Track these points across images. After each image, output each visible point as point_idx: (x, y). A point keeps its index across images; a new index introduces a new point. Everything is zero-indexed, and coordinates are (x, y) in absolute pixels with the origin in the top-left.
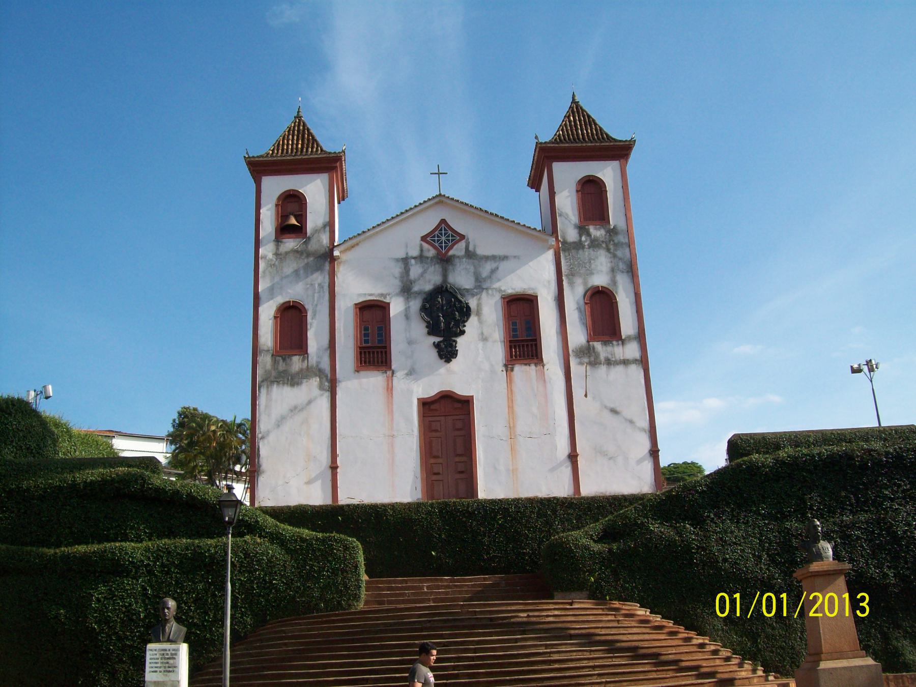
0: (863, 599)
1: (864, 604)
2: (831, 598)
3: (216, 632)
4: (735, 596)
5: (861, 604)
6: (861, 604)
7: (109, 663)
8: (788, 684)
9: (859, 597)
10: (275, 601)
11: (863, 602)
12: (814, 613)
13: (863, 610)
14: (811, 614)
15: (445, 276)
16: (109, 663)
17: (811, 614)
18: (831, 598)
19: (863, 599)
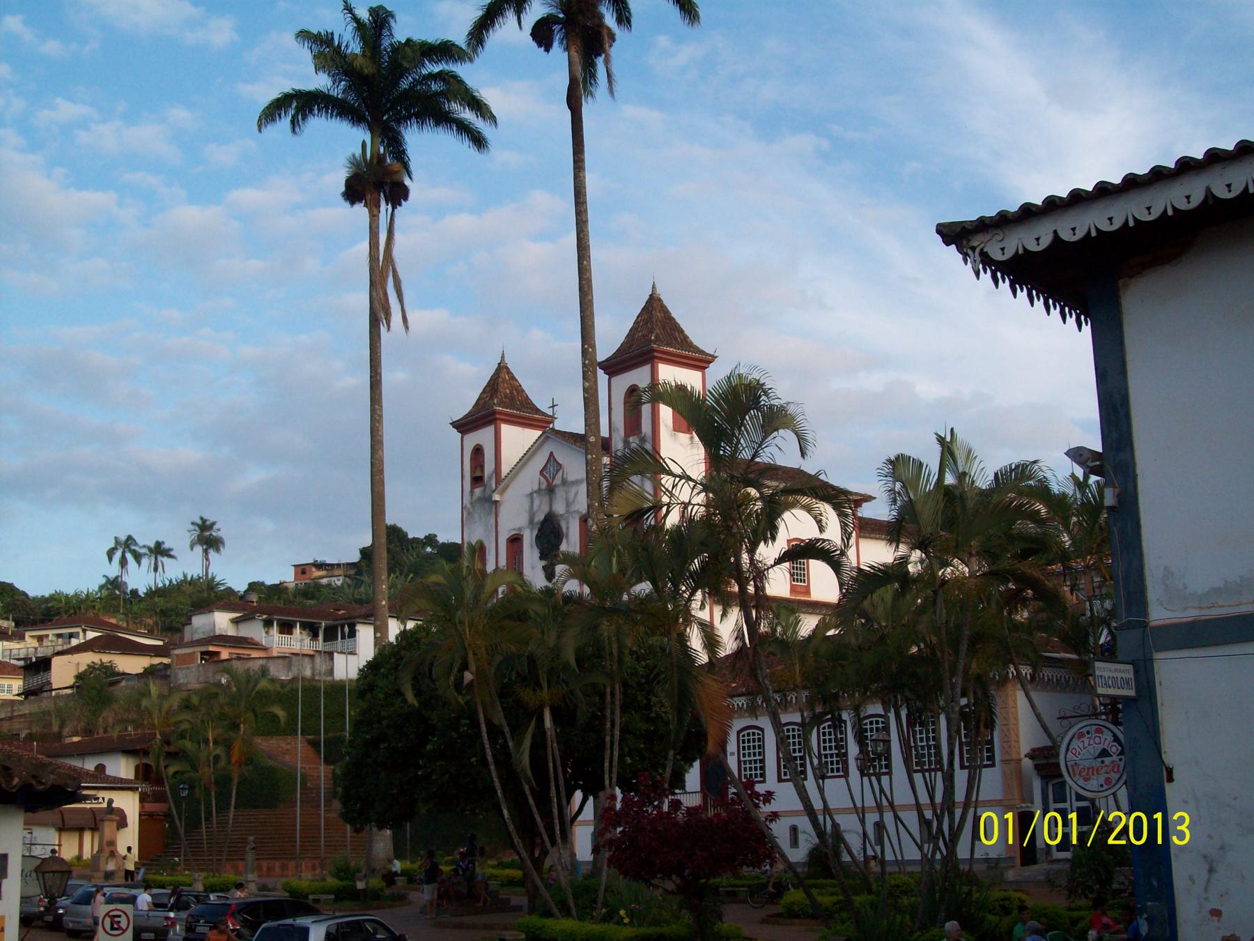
0: (1181, 820)
1: (1183, 828)
2: (1138, 820)
3: (388, 100)
4: (1070, 816)
5: (1179, 828)
6: (1179, 828)
7: (1085, 525)
8: (305, 932)
9: (1175, 817)
10: (1091, 889)
11: (1181, 824)
12: (1114, 839)
13: (1181, 836)
14: (1111, 841)
15: (551, 505)
16: (1085, 525)
17: (1111, 841)
18: (1138, 820)
19: (1181, 820)
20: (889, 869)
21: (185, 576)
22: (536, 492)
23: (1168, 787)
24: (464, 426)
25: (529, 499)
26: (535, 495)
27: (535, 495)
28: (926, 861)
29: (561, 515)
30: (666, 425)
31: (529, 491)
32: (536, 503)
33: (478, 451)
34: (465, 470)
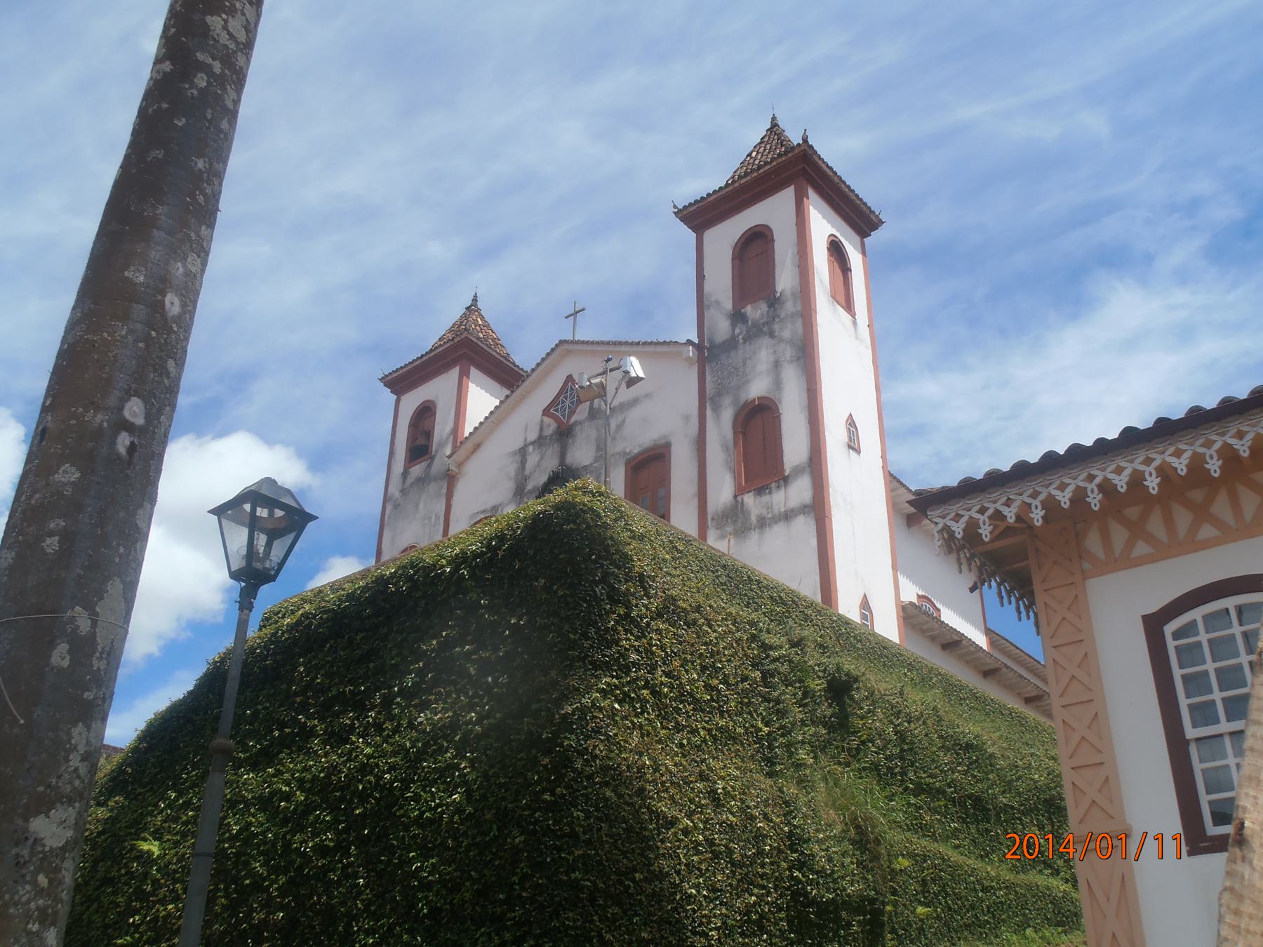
20: (586, 828)
21: (43, 839)
22: (533, 443)
23: (389, 390)
24: (400, 382)
25: (518, 458)
26: (531, 448)
27: (531, 448)
28: (463, 761)
29: (585, 467)
30: (821, 282)
31: (519, 444)
32: (533, 459)
33: (426, 412)
34: (397, 441)
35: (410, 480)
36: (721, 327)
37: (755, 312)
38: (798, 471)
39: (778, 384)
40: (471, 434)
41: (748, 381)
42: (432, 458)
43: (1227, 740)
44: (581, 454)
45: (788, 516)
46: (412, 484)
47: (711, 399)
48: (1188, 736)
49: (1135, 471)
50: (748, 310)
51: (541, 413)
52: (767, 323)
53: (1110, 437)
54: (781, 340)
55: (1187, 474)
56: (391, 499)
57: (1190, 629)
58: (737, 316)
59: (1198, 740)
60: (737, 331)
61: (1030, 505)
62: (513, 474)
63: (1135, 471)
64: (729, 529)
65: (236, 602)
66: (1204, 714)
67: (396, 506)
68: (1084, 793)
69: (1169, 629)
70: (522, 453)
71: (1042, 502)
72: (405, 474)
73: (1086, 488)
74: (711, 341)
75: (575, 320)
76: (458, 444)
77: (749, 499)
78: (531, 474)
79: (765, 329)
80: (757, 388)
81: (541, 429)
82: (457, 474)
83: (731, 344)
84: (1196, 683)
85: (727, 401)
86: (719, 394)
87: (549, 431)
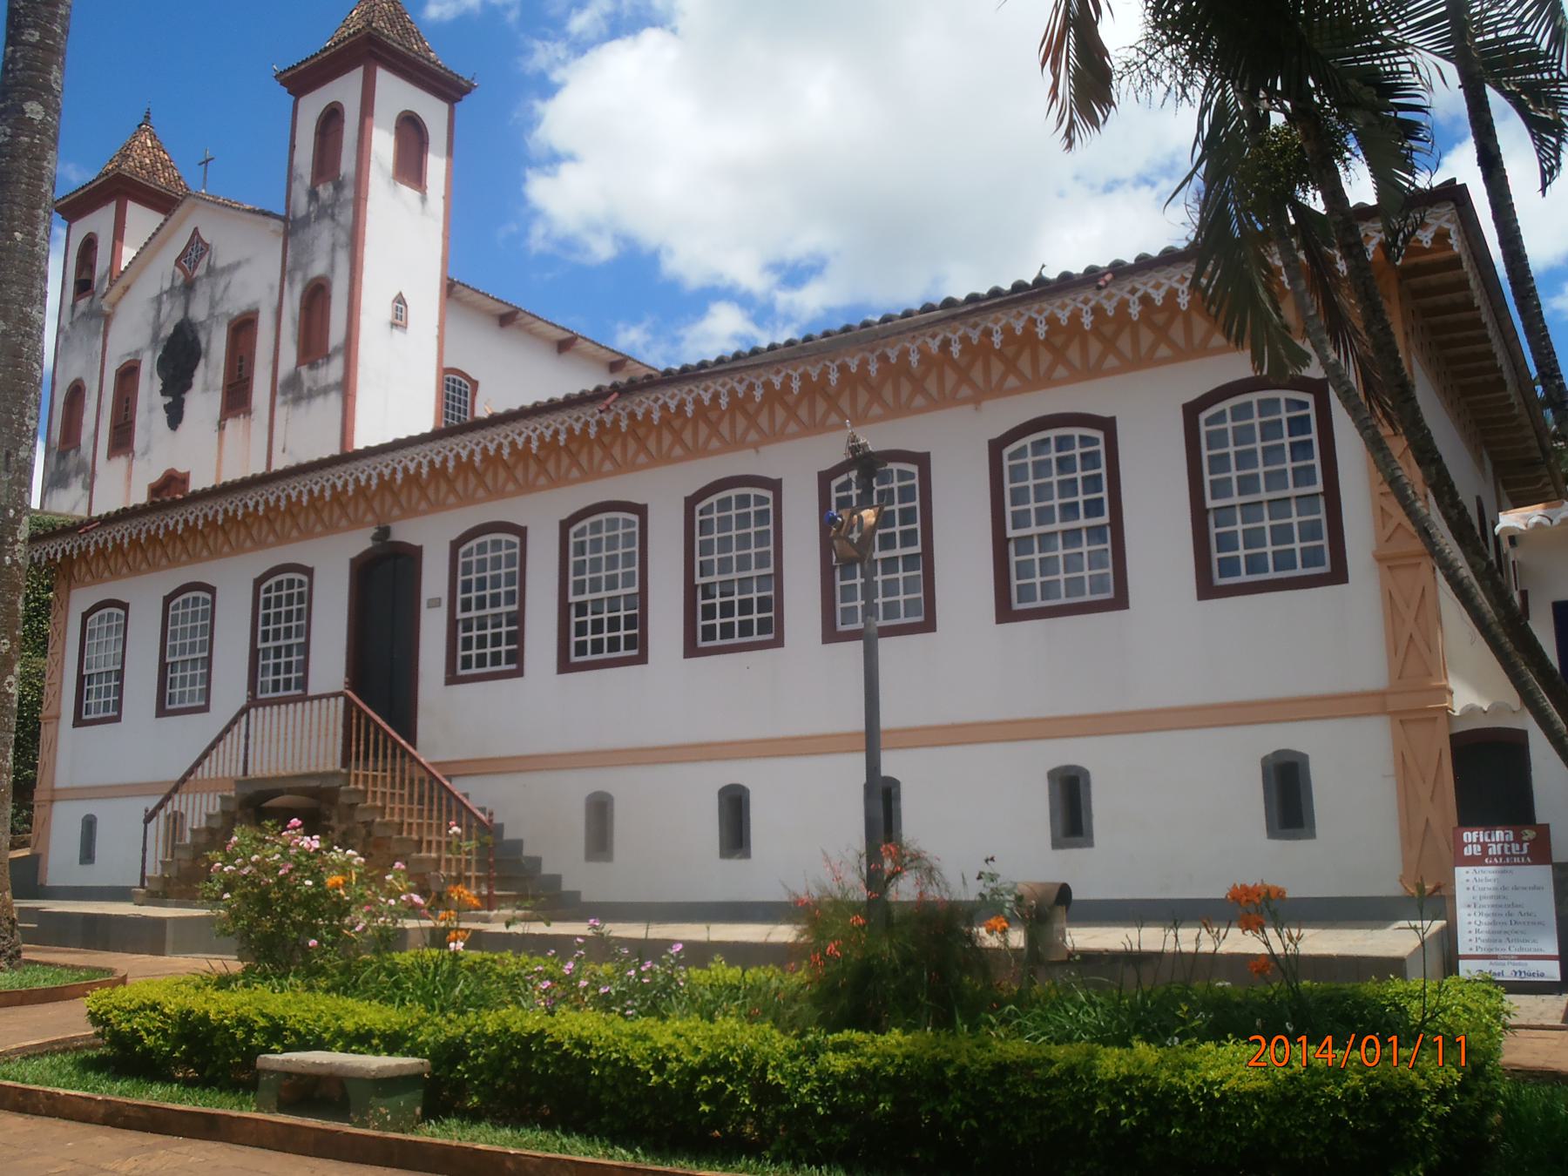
22: (166, 292)
26: (165, 296)
32: (166, 308)
35: (77, 314)
36: (301, 204)
37: (325, 191)
38: (337, 350)
39: (332, 266)
40: (126, 268)
41: (313, 261)
42: (93, 293)
43: (1293, 502)
44: (199, 312)
45: (325, 391)
46: (78, 318)
47: (290, 272)
48: (1009, 536)
49: (1171, 287)
50: (321, 188)
51: (174, 263)
52: (330, 205)
53: (1074, 271)
54: (338, 224)
55: (1162, 304)
56: (63, 330)
57: (1220, 417)
58: (313, 195)
59: (1215, 509)
60: (311, 209)
61: (1036, 320)
62: (151, 320)
63: (1171, 287)
64: (290, 396)
65: (1187, 239)
66: (1220, 489)
67: (67, 339)
68: (1391, 517)
69: (1203, 416)
70: (158, 300)
71: (1046, 318)
72: (74, 306)
73: (1082, 310)
74: (294, 217)
75: (206, 169)
76: (114, 278)
77: (304, 370)
78: (165, 322)
79: (330, 211)
80: (318, 268)
81: (173, 280)
82: (616, 237)
83: (305, 222)
84: (1302, 449)
85: (299, 276)
86: (294, 269)
87: (178, 282)
